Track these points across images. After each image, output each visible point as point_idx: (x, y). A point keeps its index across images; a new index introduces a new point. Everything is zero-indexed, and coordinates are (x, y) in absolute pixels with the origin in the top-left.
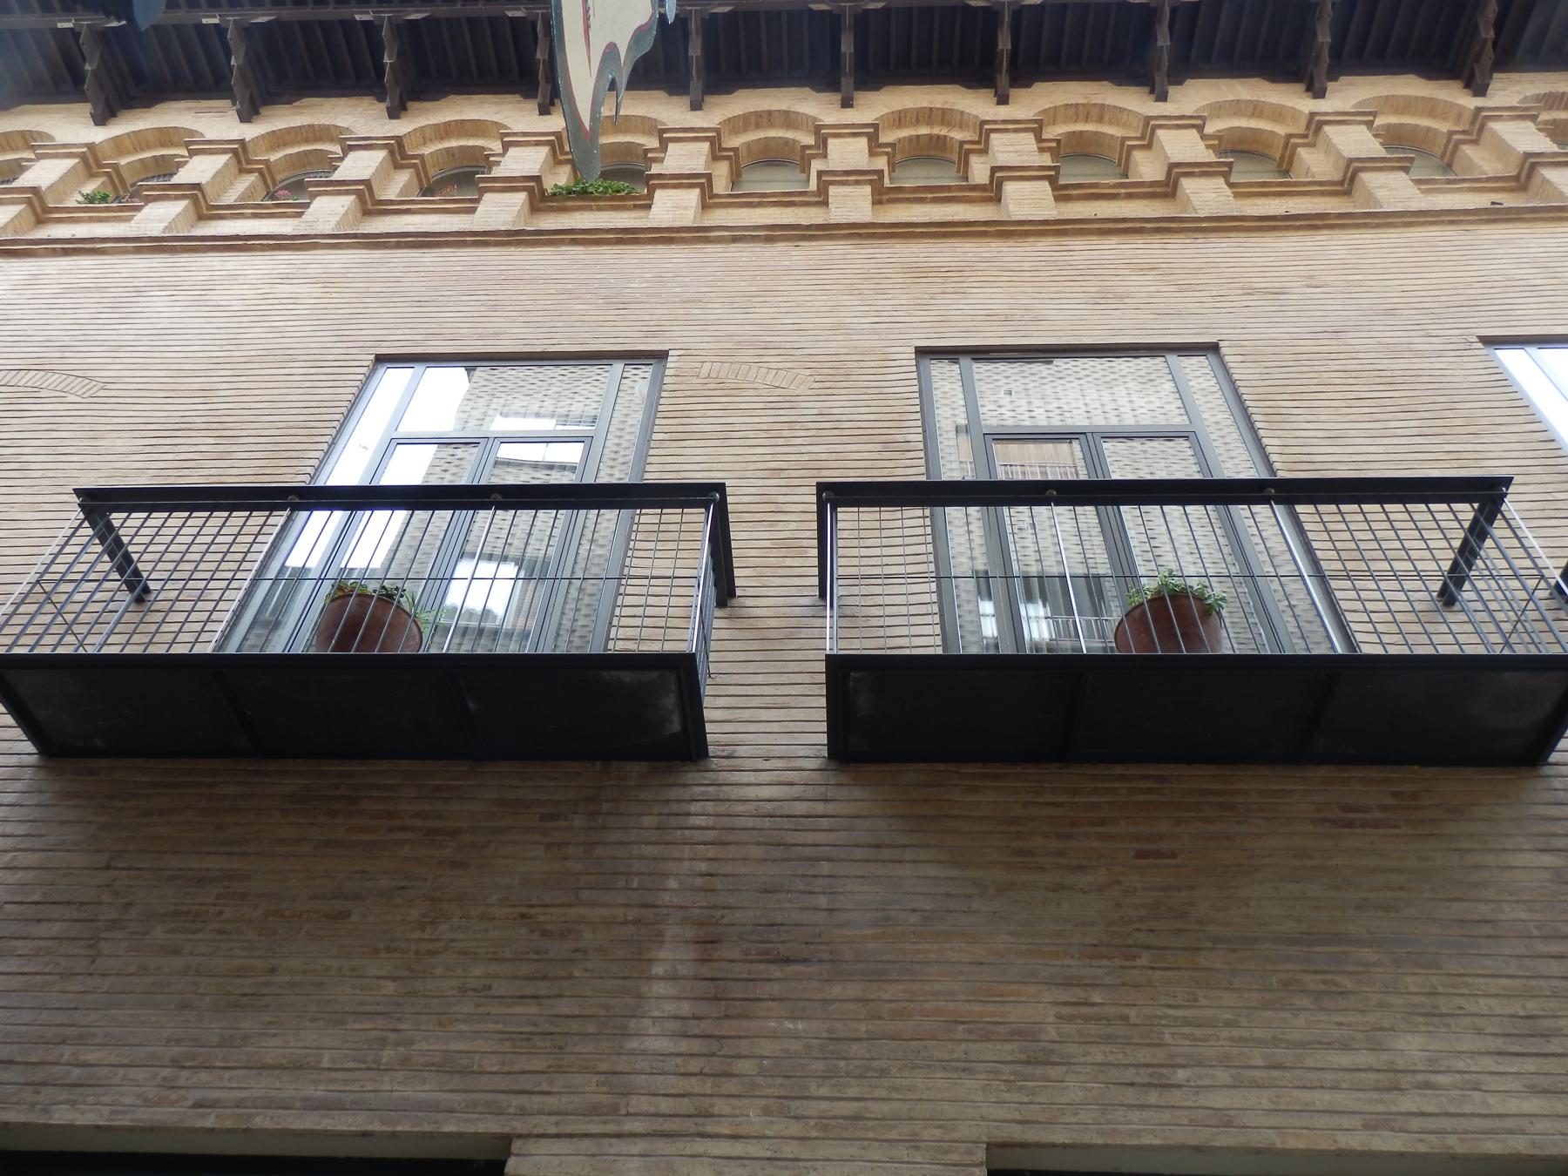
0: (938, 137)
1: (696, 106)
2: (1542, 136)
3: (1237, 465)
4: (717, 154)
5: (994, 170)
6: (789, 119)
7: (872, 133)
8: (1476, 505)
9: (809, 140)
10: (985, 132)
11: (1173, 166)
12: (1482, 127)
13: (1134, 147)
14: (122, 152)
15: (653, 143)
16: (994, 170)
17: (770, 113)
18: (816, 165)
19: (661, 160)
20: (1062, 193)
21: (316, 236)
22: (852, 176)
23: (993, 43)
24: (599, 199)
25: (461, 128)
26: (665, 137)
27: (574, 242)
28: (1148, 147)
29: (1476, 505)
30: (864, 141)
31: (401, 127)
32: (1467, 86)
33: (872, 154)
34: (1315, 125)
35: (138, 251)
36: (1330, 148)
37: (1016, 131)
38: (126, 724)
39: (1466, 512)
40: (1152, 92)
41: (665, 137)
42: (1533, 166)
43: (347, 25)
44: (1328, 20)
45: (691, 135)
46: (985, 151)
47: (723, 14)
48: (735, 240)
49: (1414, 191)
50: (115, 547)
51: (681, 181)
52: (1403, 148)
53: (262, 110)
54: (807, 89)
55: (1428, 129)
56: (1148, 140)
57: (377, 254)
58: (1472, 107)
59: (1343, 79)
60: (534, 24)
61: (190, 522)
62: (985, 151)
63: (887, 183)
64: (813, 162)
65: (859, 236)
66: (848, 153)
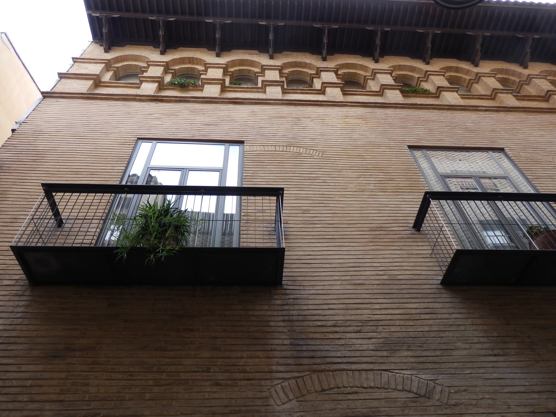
0: (505, 78)
1: (218, 55)
2: (497, 82)
3: (527, 189)
4: (225, 73)
5: (323, 83)
6: (252, 63)
7: (281, 70)
8: (54, 194)
9: (313, 72)
10: (264, 69)
11: (382, 85)
12: (375, 75)
13: (369, 79)
14: (233, 66)
15: (201, 68)
16: (323, 83)
17: (451, 67)
18: (260, 79)
19: (206, 74)
20: (345, 94)
21: (345, 102)
22: (273, 83)
23: (215, 35)
24: (420, 94)
25: (191, 60)
26: (207, 67)
27: (434, 109)
28: (373, 79)
29: (54, 194)
30: (277, 72)
31: (167, 58)
32: (521, 65)
33: (281, 77)
34: (374, 73)
35: (282, 104)
36: (433, 82)
37: (540, 78)
38: (52, 269)
39: (58, 196)
40: (374, 59)
41: (207, 67)
42: (496, 93)
43: (145, 21)
44: (379, 37)
45: (157, 64)
46: (319, 77)
47: (228, 23)
48: (486, 110)
49: (514, 99)
50: (53, 206)
51: (152, 79)
52: (455, 83)
53: (167, 50)
54: (151, 47)
55: (460, 77)
56: (318, 74)
57: (369, 110)
58: (527, 74)
59: (386, 57)
60: (159, 22)
61: (80, 198)
62: (319, 77)
63: (285, 87)
64: (259, 78)
65: (526, 111)
66: (217, 74)
